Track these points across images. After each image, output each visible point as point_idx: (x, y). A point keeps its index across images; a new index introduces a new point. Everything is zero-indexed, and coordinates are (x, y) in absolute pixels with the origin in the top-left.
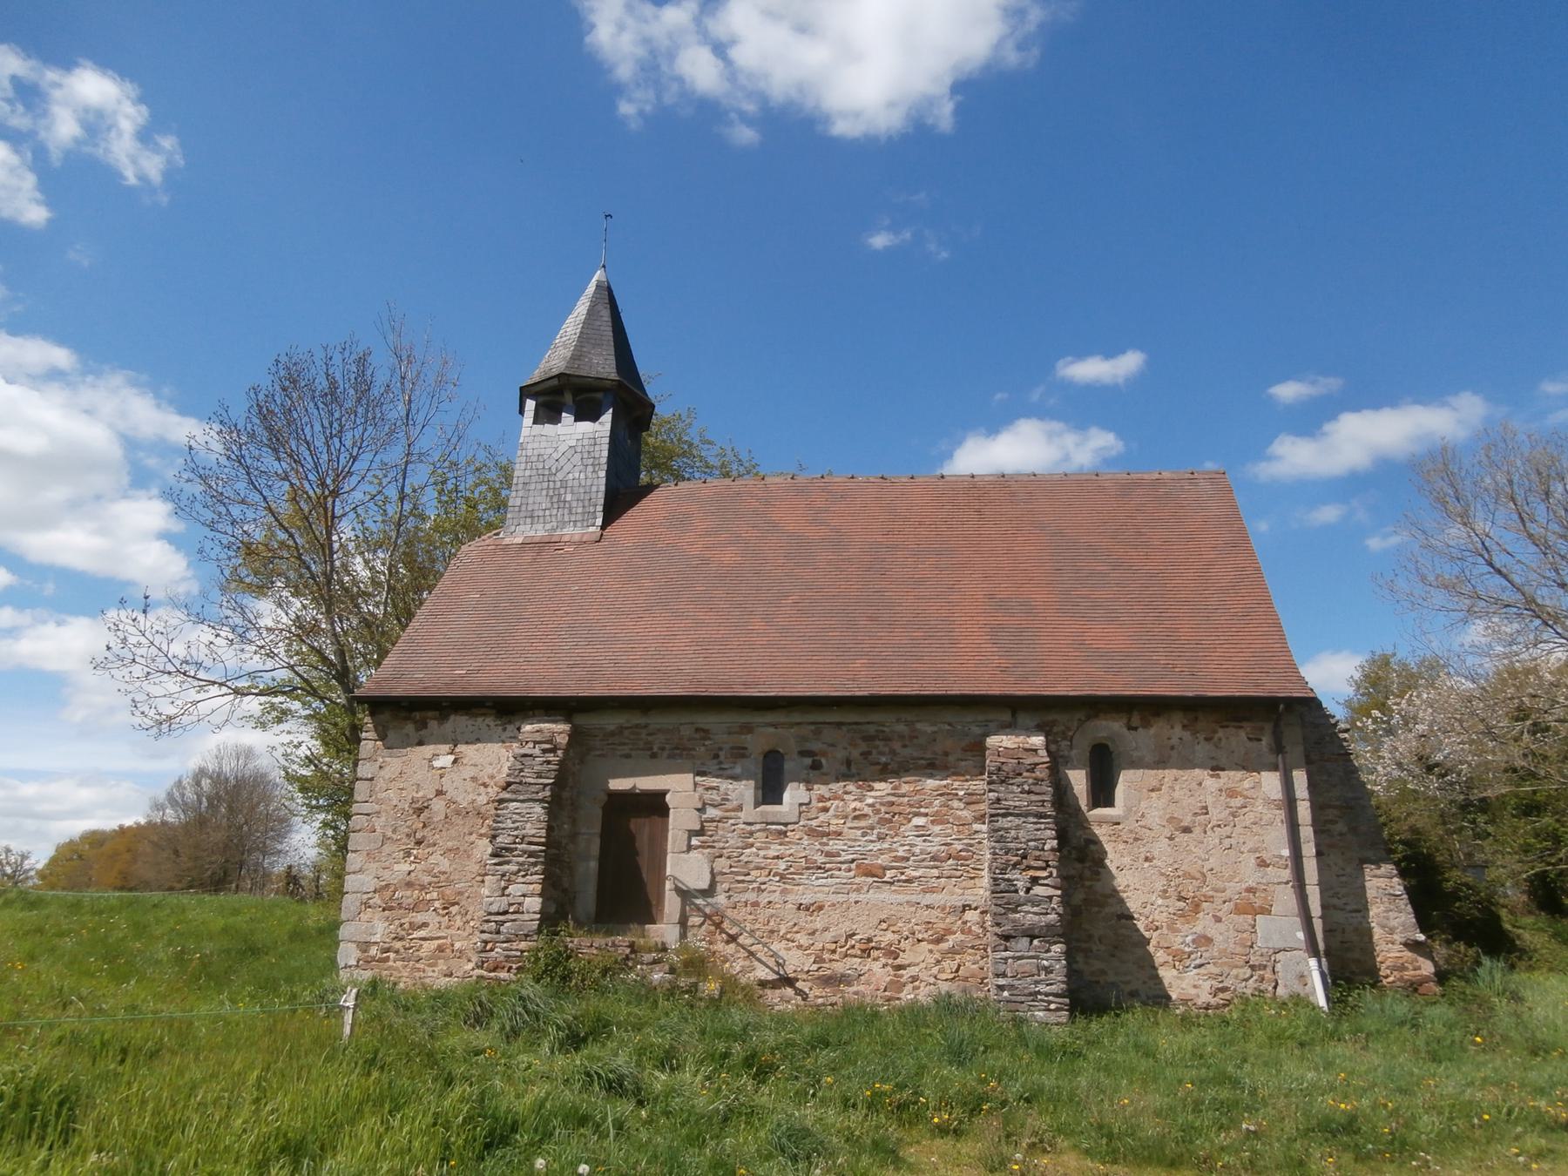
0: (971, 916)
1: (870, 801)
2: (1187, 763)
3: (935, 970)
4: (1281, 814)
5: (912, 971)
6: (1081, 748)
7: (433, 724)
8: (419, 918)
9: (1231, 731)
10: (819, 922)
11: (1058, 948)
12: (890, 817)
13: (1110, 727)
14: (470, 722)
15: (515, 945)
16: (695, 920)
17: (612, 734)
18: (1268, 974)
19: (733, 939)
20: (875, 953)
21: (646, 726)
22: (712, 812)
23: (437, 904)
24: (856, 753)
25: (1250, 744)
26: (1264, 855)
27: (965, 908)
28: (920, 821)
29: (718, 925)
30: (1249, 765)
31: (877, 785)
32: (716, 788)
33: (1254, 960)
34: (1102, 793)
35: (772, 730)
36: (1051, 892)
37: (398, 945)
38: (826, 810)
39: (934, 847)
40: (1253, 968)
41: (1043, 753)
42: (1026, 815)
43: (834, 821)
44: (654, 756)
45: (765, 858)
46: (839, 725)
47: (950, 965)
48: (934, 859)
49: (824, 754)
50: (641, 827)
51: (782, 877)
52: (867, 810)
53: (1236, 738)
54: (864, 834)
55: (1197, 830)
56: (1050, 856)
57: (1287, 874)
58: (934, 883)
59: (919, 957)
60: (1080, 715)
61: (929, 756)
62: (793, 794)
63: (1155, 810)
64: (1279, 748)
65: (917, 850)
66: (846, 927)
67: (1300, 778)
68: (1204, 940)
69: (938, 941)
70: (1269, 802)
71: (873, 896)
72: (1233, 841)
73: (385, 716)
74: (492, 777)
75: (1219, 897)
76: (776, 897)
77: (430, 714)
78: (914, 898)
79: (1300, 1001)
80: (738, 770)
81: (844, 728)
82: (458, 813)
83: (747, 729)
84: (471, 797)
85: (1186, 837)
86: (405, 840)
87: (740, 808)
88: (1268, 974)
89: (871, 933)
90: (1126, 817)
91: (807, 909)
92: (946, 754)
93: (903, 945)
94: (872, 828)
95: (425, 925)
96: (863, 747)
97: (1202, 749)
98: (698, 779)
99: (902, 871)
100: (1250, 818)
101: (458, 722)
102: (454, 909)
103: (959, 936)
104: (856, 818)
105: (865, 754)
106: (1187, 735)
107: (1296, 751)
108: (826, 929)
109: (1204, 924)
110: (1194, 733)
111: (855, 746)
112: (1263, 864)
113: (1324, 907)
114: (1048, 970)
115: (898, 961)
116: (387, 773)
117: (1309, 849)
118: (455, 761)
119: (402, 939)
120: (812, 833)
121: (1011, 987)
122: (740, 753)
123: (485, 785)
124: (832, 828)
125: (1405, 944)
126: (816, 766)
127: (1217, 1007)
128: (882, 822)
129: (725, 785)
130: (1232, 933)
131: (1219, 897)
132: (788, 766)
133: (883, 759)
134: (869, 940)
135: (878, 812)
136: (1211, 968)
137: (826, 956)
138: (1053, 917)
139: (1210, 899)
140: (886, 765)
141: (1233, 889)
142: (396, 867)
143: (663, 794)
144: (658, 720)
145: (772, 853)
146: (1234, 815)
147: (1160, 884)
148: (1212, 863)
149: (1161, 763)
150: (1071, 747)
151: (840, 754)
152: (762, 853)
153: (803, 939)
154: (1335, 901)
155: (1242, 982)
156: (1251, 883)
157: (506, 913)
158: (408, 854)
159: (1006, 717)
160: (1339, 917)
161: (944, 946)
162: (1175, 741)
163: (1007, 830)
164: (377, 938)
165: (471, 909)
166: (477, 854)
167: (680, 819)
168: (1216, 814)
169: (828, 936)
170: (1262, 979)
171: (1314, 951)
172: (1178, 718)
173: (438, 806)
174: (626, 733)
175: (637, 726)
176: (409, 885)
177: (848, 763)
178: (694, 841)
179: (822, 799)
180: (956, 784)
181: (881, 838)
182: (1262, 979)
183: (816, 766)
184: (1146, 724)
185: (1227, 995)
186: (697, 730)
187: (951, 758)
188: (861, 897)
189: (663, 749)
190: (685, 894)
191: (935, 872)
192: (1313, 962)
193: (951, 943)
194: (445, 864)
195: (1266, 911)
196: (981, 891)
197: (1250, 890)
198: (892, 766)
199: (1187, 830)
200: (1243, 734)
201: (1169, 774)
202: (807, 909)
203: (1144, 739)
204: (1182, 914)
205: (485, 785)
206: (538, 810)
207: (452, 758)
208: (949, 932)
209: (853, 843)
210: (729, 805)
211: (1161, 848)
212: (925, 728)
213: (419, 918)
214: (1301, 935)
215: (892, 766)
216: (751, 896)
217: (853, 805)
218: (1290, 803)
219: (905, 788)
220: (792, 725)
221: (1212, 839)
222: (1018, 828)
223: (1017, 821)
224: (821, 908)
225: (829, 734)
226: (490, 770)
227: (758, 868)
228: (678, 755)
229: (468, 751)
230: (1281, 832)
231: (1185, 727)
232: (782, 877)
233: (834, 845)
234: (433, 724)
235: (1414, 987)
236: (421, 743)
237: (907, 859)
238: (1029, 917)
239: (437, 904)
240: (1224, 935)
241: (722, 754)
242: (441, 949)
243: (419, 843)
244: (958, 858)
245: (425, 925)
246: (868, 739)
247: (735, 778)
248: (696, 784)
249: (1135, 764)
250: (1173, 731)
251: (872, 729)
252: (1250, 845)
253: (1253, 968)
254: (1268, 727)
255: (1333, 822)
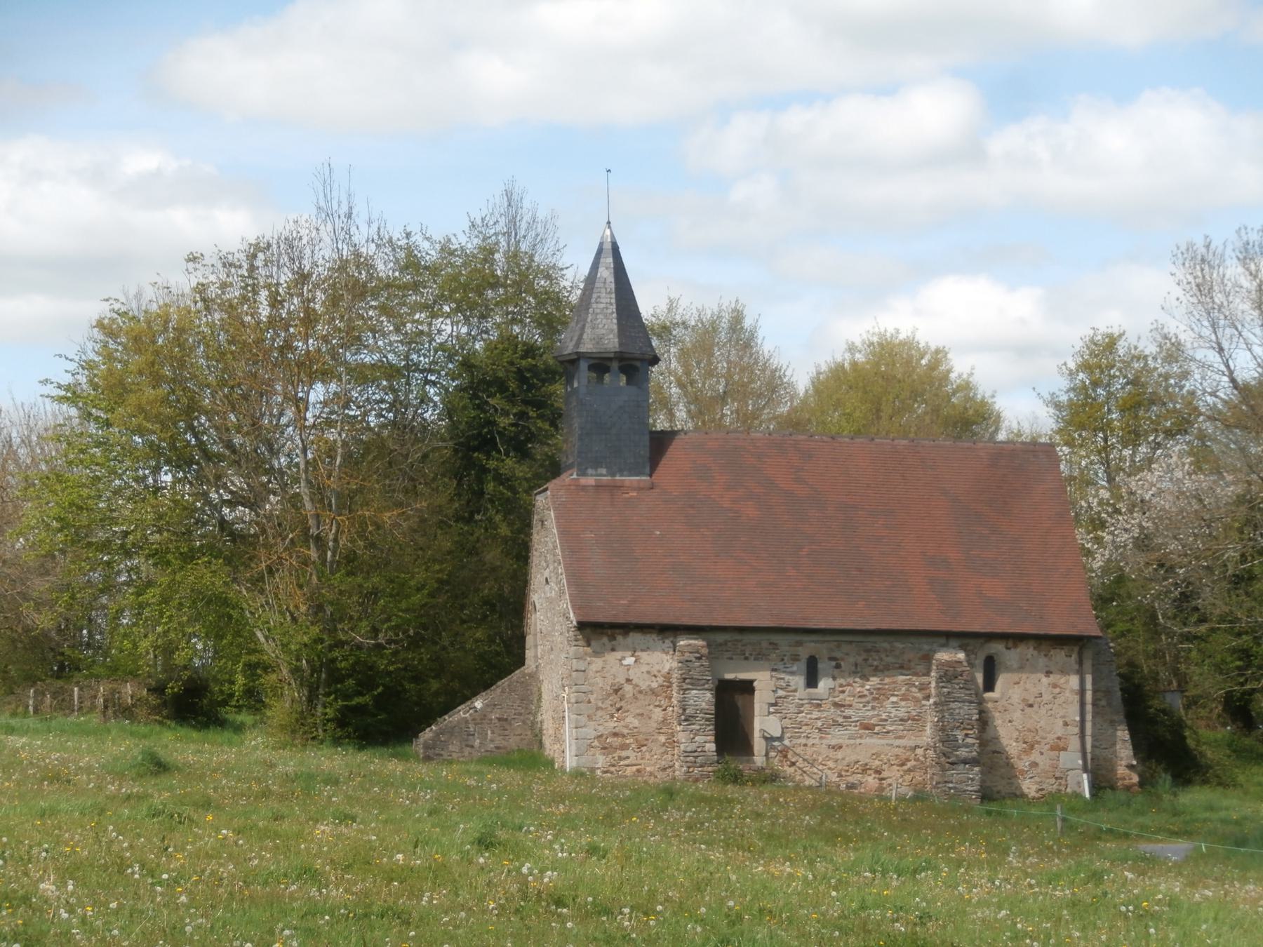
0: (919, 752)
1: (868, 687)
2: (1034, 670)
3: (900, 780)
4: (1077, 698)
5: (889, 781)
6: (979, 662)
7: (620, 638)
8: (624, 754)
9: (1058, 650)
10: (839, 755)
11: (977, 769)
12: (879, 696)
13: (997, 648)
14: (643, 637)
15: (705, 769)
16: (772, 754)
17: (721, 645)
18: (1063, 782)
19: (793, 764)
20: (869, 772)
21: (741, 641)
22: (781, 693)
23: (633, 746)
24: (860, 659)
25: (1066, 659)
26: (1067, 720)
27: (917, 747)
28: (894, 699)
29: (785, 756)
30: (1064, 671)
31: (872, 679)
32: (783, 679)
33: (1058, 774)
34: (989, 685)
35: (813, 644)
36: (974, 741)
37: (612, 769)
38: (843, 692)
39: (902, 714)
40: (1056, 778)
41: (965, 664)
42: (963, 702)
43: (848, 699)
44: (746, 658)
45: (811, 719)
46: (851, 642)
47: (908, 778)
48: (901, 720)
49: (843, 659)
50: (740, 700)
51: (820, 730)
52: (866, 693)
53: (1059, 655)
54: (864, 706)
55: (1036, 706)
56: (975, 723)
57: (1077, 730)
58: (901, 733)
59: (892, 774)
60: (982, 640)
61: (900, 661)
62: (824, 684)
63: (1016, 694)
64: (1080, 663)
65: (892, 715)
66: (854, 758)
67: (1089, 678)
68: (1034, 765)
69: (903, 765)
70: (1072, 691)
71: (868, 741)
72: (1052, 712)
73: (588, 631)
74: (659, 671)
75: (1044, 742)
76: (816, 741)
77: (617, 631)
78: (890, 742)
79: (1078, 795)
80: (795, 668)
81: (854, 645)
82: (640, 692)
83: (799, 644)
84: (647, 683)
85: (1030, 709)
86: (610, 708)
87: (795, 691)
88: (1063, 782)
89: (867, 761)
90: (1002, 698)
91: (833, 748)
92: (910, 661)
93: (884, 767)
94: (868, 702)
95: (628, 758)
96: (864, 656)
97: (1042, 661)
98: (774, 673)
99: (883, 726)
100: (1063, 699)
101: (635, 637)
102: (644, 749)
103: (913, 763)
104: (860, 697)
105: (866, 660)
106: (1035, 653)
107: (1088, 664)
108: (843, 759)
109: (1035, 756)
110: (1039, 652)
111: (859, 655)
112: (1066, 724)
113: (1093, 746)
114: (973, 780)
115: (881, 776)
116: (594, 667)
117: (1089, 717)
118: (636, 661)
119: (614, 766)
120: (836, 705)
121: (954, 788)
122: (795, 658)
123: (655, 676)
124: (847, 703)
125: (1127, 766)
126: (838, 666)
127: (1038, 798)
128: (875, 699)
129: (787, 677)
130: (1048, 761)
131: (1044, 742)
132: (820, 666)
133: (875, 663)
134: (866, 764)
135: (872, 693)
136: (1037, 779)
137: (843, 773)
138: (975, 753)
139: (1038, 743)
140: (877, 666)
141: (1051, 738)
142: (606, 724)
143: (751, 682)
144: (748, 638)
145: (814, 716)
146: (1054, 698)
147: (1015, 734)
148: (1042, 724)
149: (1021, 668)
150: (976, 659)
151: (851, 660)
152: (809, 716)
153: (831, 764)
154: (1097, 744)
155: (1051, 786)
156: (1059, 735)
157: (695, 751)
158: (612, 716)
159: (943, 640)
160: (1097, 751)
161: (905, 768)
162: (1029, 656)
163: (954, 709)
164: (599, 765)
165: (655, 748)
166: (654, 717)
167: (761, 698)
168: (1046, 697)
169: (845, 762)
170: (1060, 784)
171: (1085, 770)
172: (1032, 643)
173: (628, 688)
174: (729, 644)
175: (737, 641)
176: (615, 735)
177: (856, 665)
178: (772, 710)
179: (841, 686)
180: (914, 678)
181: (873, 708)
182: (1060, 784)
183: (838, 666)
184: (1015, 646)
185: (1043, 792)
186: (771, 644)
187: (912, 664)
188: (862, 741)
189: (751, 655)
190: (769, 739)
191: (901, 727)
192: (1085, 776)
193: (354, 703)
194: (636, 723)
195: (1065, 749)
196: (928, 734)
197: (1059, 738)
198: (881, 667)
199: (1031, 706)
200: (1063, 653)
201: (1024, 676)
202: (833, 748)
203: (1010, 656)
204: (1025, 751)
205: (655, 676)
206: (709, 696)
207: (633, 659)
208: (908, 760)
209: (859, 711)
210: (790, 688)
211: (1017, 715)
212: (899, 645)
213: (624, 754)
214: (1080, 762)
215: (881, 667)
216: (803, 741)
217: (858, 690)
218: (1082, 692)
219: (887, 680)
220: (824, 642)
221: (1043, 711)
222: (960, 708)
223: (960, 705)
224: (841, 747)
225: (845, 648)
226: (657, 667)
227: (807, 725)
228: (760, 657)
229: (644, 656)
230: (1076, 707)
231: (1035, 648)
232: (820, 730)
233: (848, 712)
234: (620, 638)
235: (1128, 788)
236: (613, 650)
237: (886, 720)
238: (963, 753)
239: (633, 746)
240: (1044, 761)
241: (786, 658)
242: (638, 771)
243: (618, 710)
244: (913, 720)
245: (628, 758)
246: (867, 651)
247: (792, 673)
248: (772, 676)
249: (1009, 669)
250: (1028, 651)
251: (869, 646)
252: (1061, 714)
253: (1056, 778)
254: (1076, 649)
255: (1100, 700)
